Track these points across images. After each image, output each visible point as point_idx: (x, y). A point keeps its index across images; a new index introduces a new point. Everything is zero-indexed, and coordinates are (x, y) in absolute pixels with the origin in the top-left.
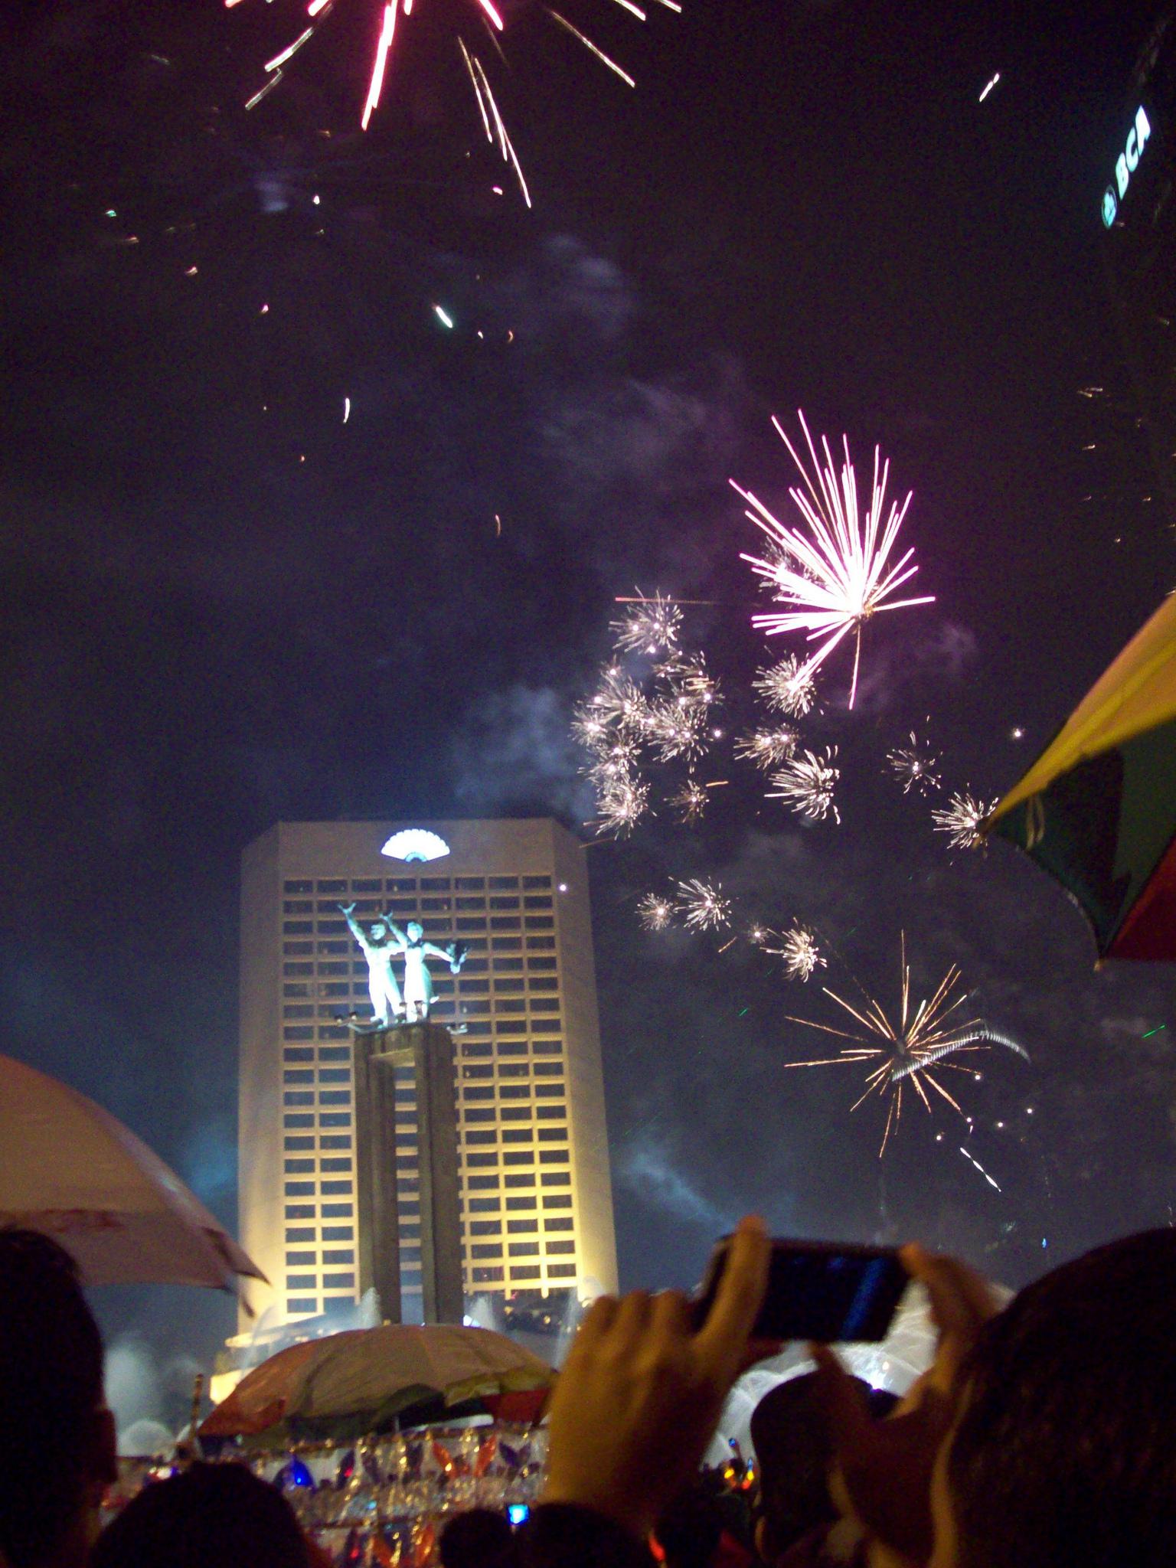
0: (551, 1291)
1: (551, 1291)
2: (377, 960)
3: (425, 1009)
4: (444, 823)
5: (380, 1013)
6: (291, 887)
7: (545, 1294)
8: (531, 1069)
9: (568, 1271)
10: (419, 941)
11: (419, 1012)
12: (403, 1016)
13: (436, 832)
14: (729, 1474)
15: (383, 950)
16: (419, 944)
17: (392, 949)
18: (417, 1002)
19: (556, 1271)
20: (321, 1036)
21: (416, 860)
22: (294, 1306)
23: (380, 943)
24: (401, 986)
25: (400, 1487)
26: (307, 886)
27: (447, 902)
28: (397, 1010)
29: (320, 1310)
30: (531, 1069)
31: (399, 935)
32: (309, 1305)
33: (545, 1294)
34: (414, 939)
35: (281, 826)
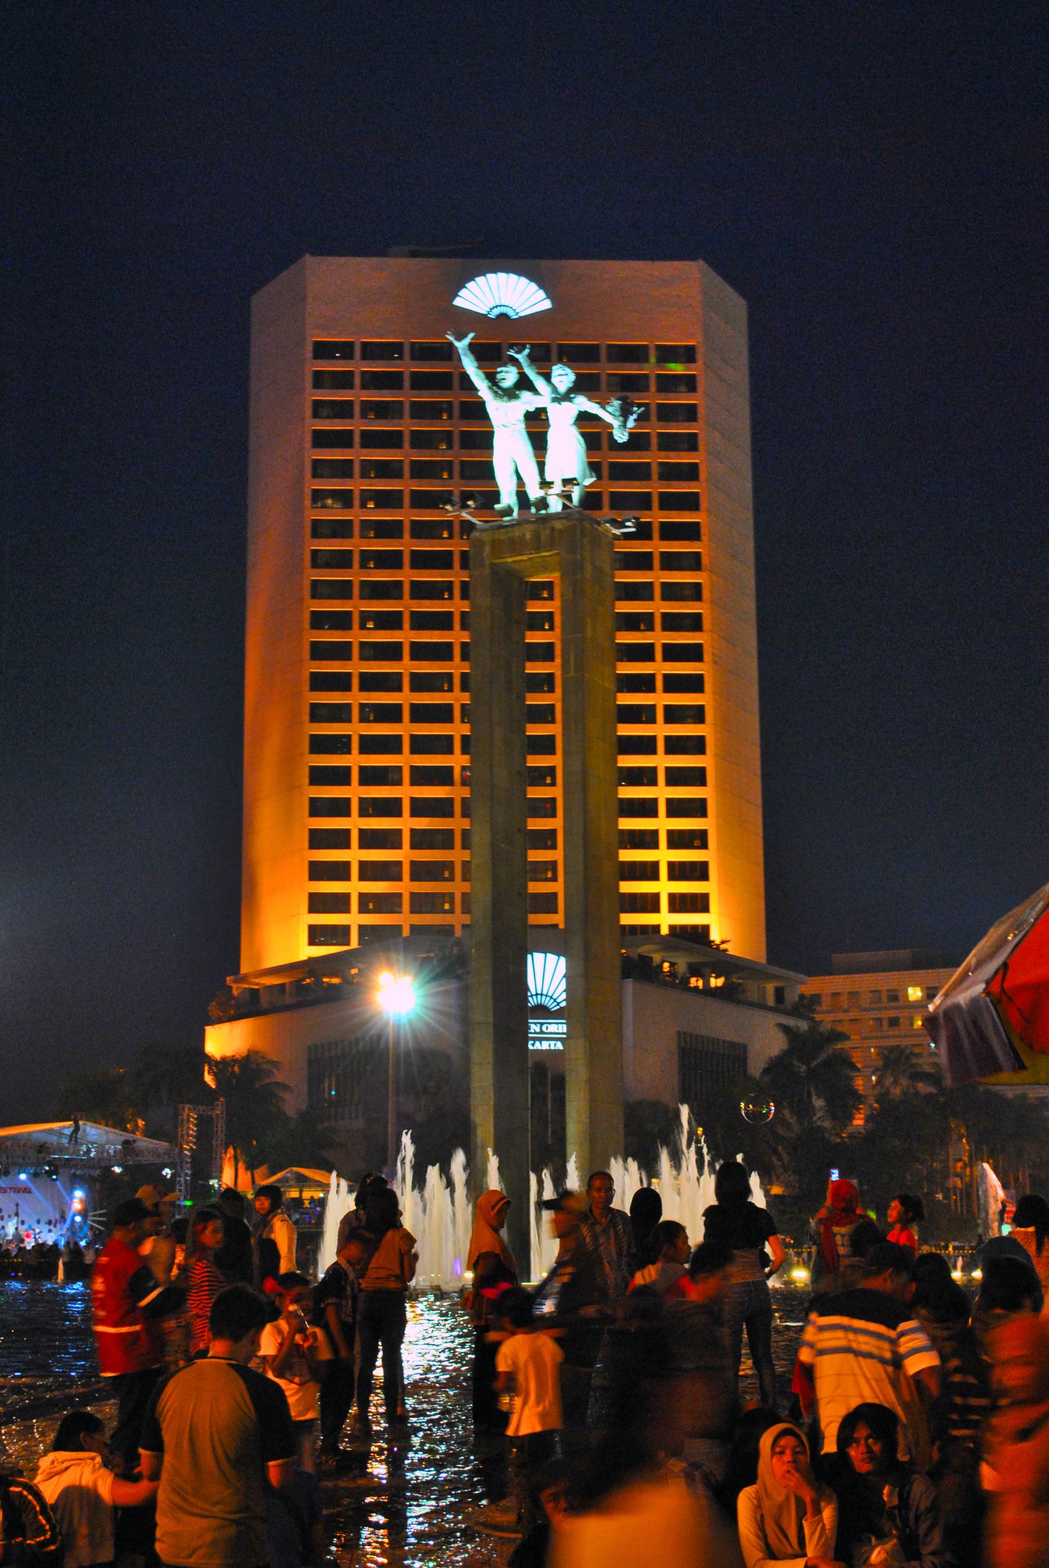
0: (672, 928)
1: (672, 928)
2: (506, 418)
3: (576, 494)
4: (546, 264)
5: (508, 498)
6: (323, 350)
7: (664, 931)
8: (658, 621)
9: (699, 903)
10: (571, 390)
11: (567, 497)
12: (543, 503)
13: (532, 278)
14: (298, 1338)
15: (514, 403)
16: (566, 397)
17: (527, 402)
18: (566, 482)
19: (680, 903)
20: (363, 566)
21: (503, 316)
22: (316, 935)
23: (510, 394)
24: (541, 466)
25: (158, 1272)
26: (346, 350)
27: (448, 437)
28: (534, 492)
29: (354, 943)
30: (658, 621)
31: (539, 382)
32: (339, 934)
33: (664, 931)
34: (562, 388)
35: (309, 259)
